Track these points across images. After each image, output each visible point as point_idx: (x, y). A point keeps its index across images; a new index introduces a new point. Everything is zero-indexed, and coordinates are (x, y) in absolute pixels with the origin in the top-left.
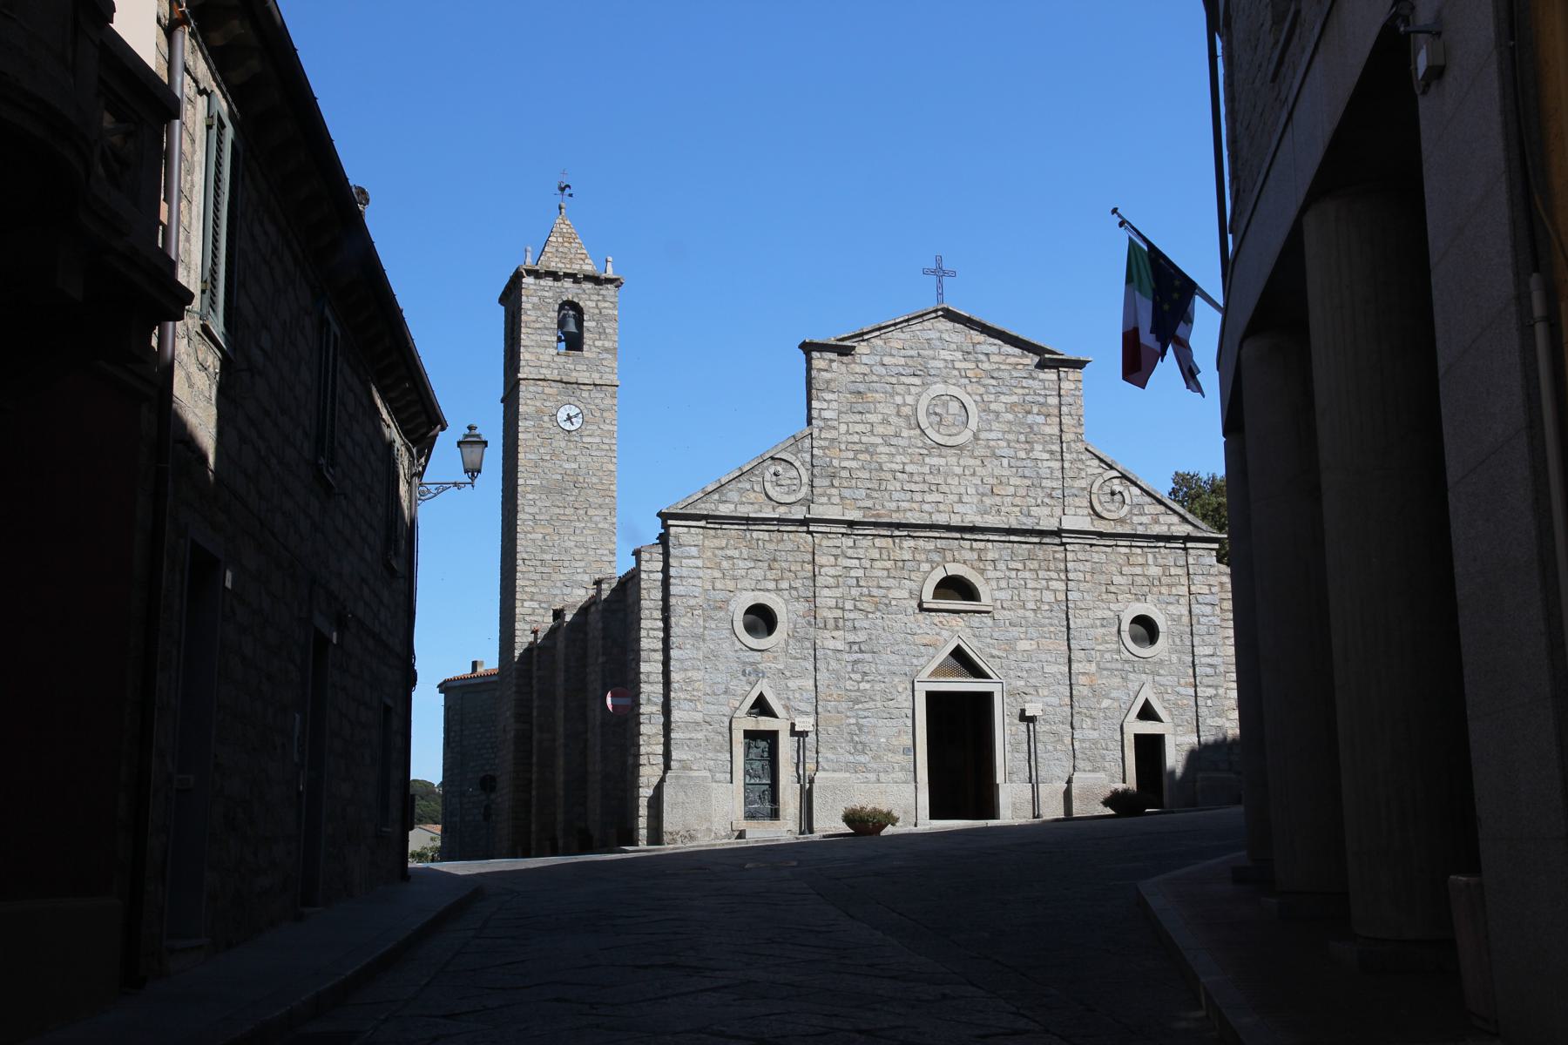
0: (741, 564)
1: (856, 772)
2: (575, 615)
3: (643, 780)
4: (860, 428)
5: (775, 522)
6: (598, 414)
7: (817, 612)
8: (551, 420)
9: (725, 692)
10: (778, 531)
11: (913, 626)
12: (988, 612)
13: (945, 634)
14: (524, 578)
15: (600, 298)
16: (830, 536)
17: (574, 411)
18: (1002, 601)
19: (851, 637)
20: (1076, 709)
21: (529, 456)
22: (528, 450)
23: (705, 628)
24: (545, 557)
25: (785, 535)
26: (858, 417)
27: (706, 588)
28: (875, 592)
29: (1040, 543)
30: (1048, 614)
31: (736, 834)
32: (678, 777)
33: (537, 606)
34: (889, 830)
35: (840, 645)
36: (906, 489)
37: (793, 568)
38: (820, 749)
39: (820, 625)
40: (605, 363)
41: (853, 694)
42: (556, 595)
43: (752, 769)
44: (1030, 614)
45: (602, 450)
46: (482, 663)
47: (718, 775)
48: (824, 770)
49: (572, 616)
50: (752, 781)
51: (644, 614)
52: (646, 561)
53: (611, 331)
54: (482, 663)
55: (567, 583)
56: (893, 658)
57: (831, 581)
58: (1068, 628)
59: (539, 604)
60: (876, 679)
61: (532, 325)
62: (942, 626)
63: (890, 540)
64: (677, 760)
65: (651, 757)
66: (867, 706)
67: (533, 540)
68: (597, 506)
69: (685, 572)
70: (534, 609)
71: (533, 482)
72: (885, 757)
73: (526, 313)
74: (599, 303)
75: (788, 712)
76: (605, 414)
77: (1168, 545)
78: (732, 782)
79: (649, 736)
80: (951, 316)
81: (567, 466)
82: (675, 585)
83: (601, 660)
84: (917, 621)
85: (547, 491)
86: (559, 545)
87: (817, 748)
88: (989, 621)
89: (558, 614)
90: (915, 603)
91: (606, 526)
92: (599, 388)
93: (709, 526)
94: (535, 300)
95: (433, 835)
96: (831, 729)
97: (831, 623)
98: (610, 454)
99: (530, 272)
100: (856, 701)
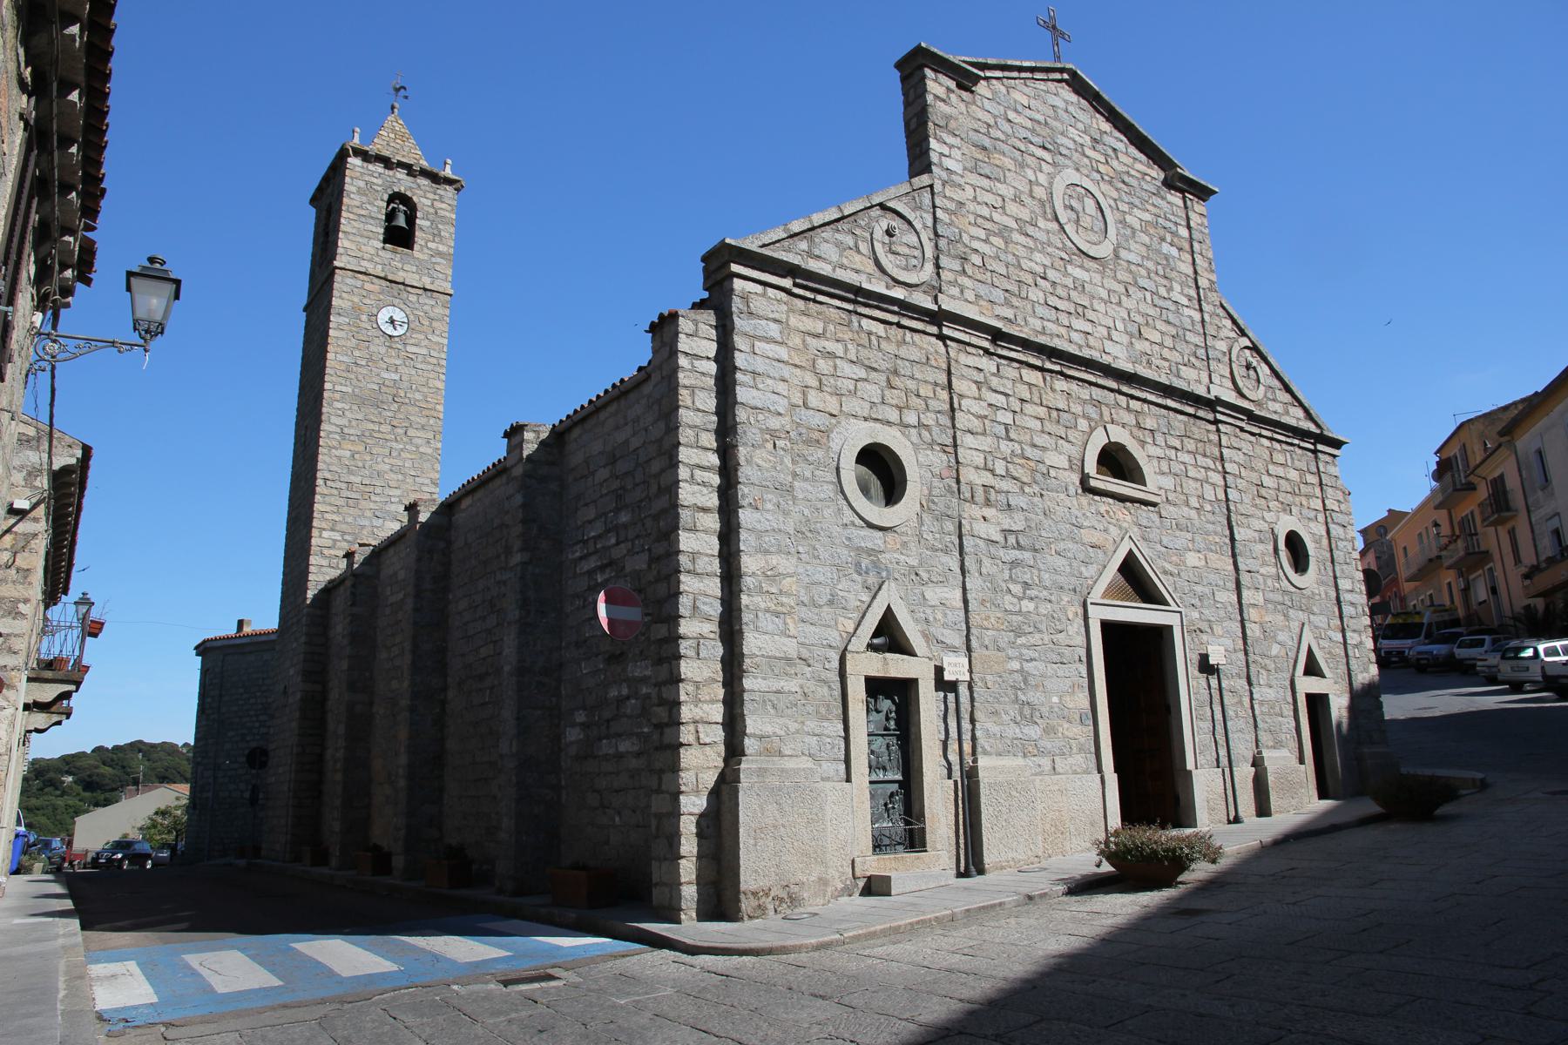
0: (847, 369)
2: (433, 513)
3: (686, 778)
4: (990, 199)
5: (896, 308)
6: (426, 323)
8: (369, 320)
9: (831, 603)
10: (899, 325)
12: (1154, 505)
14: (324, 503)
15: (437, 197)
16: (969, 349)
17: (399, 316)
20: (1252, 657)
21: (340, 357)
22: (339, 350)
23: (795, 475)
24: (352, 479)
25: (908, 334)
26: (985, 183)
27: (794, 401)
28: (1029, 452)
29: (1195, 416)
30: (1210, 516)
31: (861, 883)
32: (762, 772)
33: (340, 538)
36: (1050, 303)
37: (922, 393)
40: (438, 268)
42: (363, 527)
44: (1193, 514)
45: (429, 363)
46: (249, 622)
48: (985, 753)
49: (428, 515)
51: (685, 435)
52: (688, 335)
53: (447, 235)
54: (249, 622)
55: (378, 514)
57: (976, 424)
58: (1233, 539)
59: (342, 536)
61: (355, 210)
63: (1039, 374)
64: (754, 735)
65: (701, 728)
67: (339, 458)
68: (420, 426)
69: (760, 365)
70: (335, 541)
71: (344, 389)
72: (1060, 729)
73: (348, 195)
74: (435, 203)
76: (435, 324)
77: (1303, 444)
78: (848, 780)
79: (697, 684)
80: (1077, 85)
81: (385, 375)
82: (743, 385)
83: (517, 558)
84: (1081, 507)
85: (361, 401)
86: (371, 467)
88: (1155, 517)
89: (412, 509)
91: (429, 451)
92: (429, 294)
93: (797, 291)
94: (362, 184)
95: (177, 794)
98: (438, 369)
99: (358, 153)
100: (1018, 632)
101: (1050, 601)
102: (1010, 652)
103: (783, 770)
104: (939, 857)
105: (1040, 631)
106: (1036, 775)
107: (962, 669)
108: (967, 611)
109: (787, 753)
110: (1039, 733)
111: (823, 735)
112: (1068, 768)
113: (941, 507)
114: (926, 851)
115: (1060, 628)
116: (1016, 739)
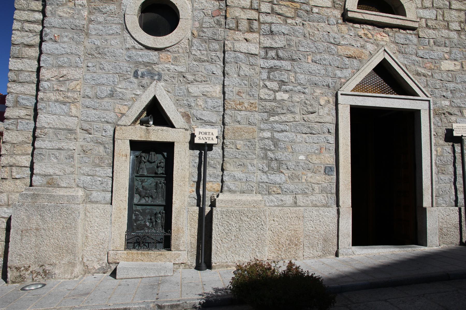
1: (269, 194)
7: (228, 11)
11: (337, 36)
12: (413, 29)
13: (370, 47)
18: (426, 20)
19: (267, 42)
34: (141, 151)
35: (254, 49)
38: (227, 166)
39: (231, 25)
41: (268, 104)
44: (454, 35)
47: (95, 194)
50: (143, 201)
56: (314, 67)
62: (366, 39)
66: (284, 118)
78: (111, 204)
88: (414, 39)
90: (338, 13)
96: (240, 144)
97: (244, 25)
101: (304, 93)
103: (51, 196)
104: (179, 255)
105: (292, 112)
106: (278, 206)
107: (211, 136)
109: (63, 185)
111: (95, 175)
113: (209, 33)
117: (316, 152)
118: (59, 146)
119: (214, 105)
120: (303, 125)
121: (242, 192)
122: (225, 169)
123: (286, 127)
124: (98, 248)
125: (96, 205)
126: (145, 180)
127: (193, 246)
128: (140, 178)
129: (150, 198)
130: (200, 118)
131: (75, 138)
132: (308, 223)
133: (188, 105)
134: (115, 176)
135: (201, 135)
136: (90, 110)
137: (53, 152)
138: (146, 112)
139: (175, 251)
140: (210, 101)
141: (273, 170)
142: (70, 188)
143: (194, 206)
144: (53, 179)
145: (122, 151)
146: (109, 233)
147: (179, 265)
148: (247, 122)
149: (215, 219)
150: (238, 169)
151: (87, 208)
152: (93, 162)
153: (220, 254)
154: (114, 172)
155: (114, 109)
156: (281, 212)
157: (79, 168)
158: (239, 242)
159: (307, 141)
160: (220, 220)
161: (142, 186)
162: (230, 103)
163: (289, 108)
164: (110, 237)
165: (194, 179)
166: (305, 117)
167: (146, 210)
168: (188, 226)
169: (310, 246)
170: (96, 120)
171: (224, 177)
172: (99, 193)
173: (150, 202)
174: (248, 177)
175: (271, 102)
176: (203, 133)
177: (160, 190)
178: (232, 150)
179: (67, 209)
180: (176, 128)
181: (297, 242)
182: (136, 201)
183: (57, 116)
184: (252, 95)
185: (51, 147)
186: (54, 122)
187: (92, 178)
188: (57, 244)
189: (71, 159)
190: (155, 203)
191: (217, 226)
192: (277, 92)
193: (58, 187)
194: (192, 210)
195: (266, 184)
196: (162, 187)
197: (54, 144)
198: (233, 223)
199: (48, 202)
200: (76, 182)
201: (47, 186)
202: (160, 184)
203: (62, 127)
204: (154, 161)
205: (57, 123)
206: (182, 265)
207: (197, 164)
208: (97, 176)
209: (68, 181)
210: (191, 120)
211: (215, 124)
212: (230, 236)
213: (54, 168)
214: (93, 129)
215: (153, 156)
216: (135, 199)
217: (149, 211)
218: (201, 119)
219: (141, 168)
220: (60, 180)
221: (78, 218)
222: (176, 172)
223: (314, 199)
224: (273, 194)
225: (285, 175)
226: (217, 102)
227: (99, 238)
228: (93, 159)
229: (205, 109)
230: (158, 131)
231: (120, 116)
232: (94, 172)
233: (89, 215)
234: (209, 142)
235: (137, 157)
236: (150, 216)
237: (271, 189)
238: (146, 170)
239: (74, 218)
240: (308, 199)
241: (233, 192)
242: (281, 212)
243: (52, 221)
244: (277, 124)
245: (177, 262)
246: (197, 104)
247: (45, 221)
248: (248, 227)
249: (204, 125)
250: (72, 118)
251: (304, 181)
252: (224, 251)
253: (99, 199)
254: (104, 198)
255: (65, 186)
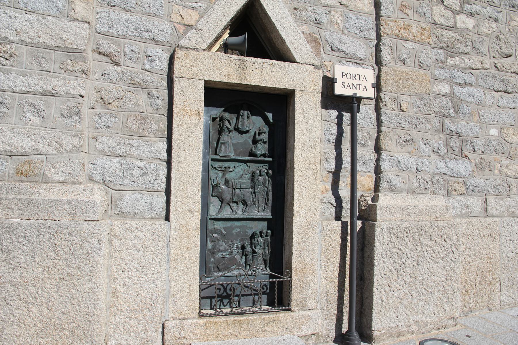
1: (448, 193)
34: (223, 109)
38: (385, 142)
41: (445, 33)
43: (226, 182)
47: (129, 197)
48: (392, 189)
50: (227, 212)
60: (484, 11)
66: (469, 62)
72: (498, 166)
75: (318, 54)
78: (167, 219)
87: (378, 140)
96: (406, 102)
101: (496, 20)
102: (438, 73)
103: (28, 203)
104: (307, 319)
105: (479, 52)
106: (461, 216)
107: (364, 83)
108: (378, 16)
109: (55, 177)
110: (469, 168)
111: (129, 156)
112: (504, 209)
114: (290, 310)
115: (506, 51)
116: (439, 174)
117: (513, 123)
118: (45, 87)
119: (361, 25)
120: (495, 77)
121: (411, 191)
122: (383, 148)
123: (471, 78)
124: (140, 317)
125: (135, 222)
126: (229, 168)
127: (331, 299)
128: (220, 164)
129: (241, 205)
130: (338, 49)
131: (83, 70)
132: (506, 245)
133: (316, 20)
134: (176, 157)
135: (345, 79)
136: (116, 11)
137: (31, 98)
138: (228, 31)
139: (298, 311)
140: (354, 17)
141: (453, 152)
142: (73, 183)
143: (330, 220)
144: (30, 162)
145: (189, 102)
146: (164, 282)
147: (306, 338)
148: (417, 63)
149: (379, 244)
150: (404, 149)
151: (113, 230)
152: (125, 125)
153: (386, 313)
154: (173, 150)
155: (169, 14)
156: (469, 227)
157: (93, 138)
158: (417, 286)
159: (500, 105)
160: (387, 246)
161: (224, 180)
162: (389, 24)
163: (474, 44)
164: (167, 291)
165: (329, 166)
166: (499, 62)
167: (233, 229)
168: (321, 259)
169: (509, 285)
170: (130, 33)
171: (381, 163)
172: (139, 196)
173: (240, 212)
174: (420, 164)
175: (450, 30)
176: (349, 76)
177: (259, 189)
178: (393, 112)
179: (69, 233)
180: (297, 63)
181: (491, 279)
182: (213, 212)
183: (39, 17)
184: (422, 14)
185: (26, 87)
186: (31, 30)
187: (122, 162)
188: (48, 318)
189: (75, 118)
190: (252, 215)
191: (382, 259)
192: (458, 14)
193: (44, 180)
194: (329, 228)
195: (444, 177)
196: (264, 183)
197: (32, 82)
198: (408, 251)
199: (22, 216)
200: (86, 170)
201: (18, 178)
202: (260, 175)
203: (53, 43)
204: (248, 129)
205: (40, 33)
206: (313, 336)
207: (335, 137)
208: (134, 157)
209: (69, 168)
210: (322, 50)
211: (363, 62)
212: (402, 276)
213: (33, 138)
214: (122, 54)
215: (246, 118)
216: (211, 207)
217: (240, 232)
218: (339, 50)
219: (222, 143)
220: (49, 165)
221: (97, 253)
222: (300, 152)
223: (511, 204)
224: (454, 195)
225: (471, 162)
226: (365, 21)
227: (144, 295)
228: (125, 120)
229: (345, 31)
230: (263, 66)
231: (182, 31)
232: (128, 148)
233: (118, 245)
234: (360, 94)
235: (214, 119)
236: (240, 241)
237: (451, 186)
238: (233, 147)
239: (88, 253)
240: (503, 203)
241: (397, 191)
242: (469, 227)
243: (34, 263)
244: (458, 71)
245: (304, 334)
246: (331, 21)
247: (14, 263)
248: (431, 257)
249: (345, 62)
250: (76, 23)
251: (497, 172)
252: (393, 305)
253: (140, 208)
254: (149, 206)
255: (61, 179)
